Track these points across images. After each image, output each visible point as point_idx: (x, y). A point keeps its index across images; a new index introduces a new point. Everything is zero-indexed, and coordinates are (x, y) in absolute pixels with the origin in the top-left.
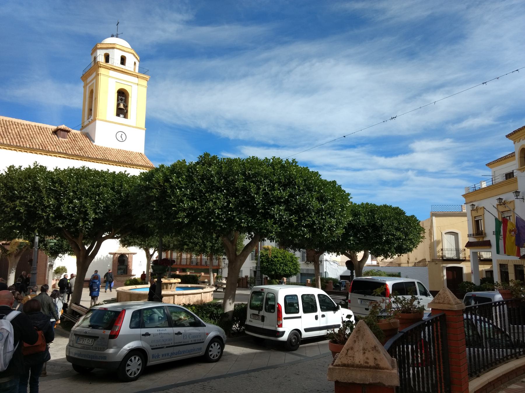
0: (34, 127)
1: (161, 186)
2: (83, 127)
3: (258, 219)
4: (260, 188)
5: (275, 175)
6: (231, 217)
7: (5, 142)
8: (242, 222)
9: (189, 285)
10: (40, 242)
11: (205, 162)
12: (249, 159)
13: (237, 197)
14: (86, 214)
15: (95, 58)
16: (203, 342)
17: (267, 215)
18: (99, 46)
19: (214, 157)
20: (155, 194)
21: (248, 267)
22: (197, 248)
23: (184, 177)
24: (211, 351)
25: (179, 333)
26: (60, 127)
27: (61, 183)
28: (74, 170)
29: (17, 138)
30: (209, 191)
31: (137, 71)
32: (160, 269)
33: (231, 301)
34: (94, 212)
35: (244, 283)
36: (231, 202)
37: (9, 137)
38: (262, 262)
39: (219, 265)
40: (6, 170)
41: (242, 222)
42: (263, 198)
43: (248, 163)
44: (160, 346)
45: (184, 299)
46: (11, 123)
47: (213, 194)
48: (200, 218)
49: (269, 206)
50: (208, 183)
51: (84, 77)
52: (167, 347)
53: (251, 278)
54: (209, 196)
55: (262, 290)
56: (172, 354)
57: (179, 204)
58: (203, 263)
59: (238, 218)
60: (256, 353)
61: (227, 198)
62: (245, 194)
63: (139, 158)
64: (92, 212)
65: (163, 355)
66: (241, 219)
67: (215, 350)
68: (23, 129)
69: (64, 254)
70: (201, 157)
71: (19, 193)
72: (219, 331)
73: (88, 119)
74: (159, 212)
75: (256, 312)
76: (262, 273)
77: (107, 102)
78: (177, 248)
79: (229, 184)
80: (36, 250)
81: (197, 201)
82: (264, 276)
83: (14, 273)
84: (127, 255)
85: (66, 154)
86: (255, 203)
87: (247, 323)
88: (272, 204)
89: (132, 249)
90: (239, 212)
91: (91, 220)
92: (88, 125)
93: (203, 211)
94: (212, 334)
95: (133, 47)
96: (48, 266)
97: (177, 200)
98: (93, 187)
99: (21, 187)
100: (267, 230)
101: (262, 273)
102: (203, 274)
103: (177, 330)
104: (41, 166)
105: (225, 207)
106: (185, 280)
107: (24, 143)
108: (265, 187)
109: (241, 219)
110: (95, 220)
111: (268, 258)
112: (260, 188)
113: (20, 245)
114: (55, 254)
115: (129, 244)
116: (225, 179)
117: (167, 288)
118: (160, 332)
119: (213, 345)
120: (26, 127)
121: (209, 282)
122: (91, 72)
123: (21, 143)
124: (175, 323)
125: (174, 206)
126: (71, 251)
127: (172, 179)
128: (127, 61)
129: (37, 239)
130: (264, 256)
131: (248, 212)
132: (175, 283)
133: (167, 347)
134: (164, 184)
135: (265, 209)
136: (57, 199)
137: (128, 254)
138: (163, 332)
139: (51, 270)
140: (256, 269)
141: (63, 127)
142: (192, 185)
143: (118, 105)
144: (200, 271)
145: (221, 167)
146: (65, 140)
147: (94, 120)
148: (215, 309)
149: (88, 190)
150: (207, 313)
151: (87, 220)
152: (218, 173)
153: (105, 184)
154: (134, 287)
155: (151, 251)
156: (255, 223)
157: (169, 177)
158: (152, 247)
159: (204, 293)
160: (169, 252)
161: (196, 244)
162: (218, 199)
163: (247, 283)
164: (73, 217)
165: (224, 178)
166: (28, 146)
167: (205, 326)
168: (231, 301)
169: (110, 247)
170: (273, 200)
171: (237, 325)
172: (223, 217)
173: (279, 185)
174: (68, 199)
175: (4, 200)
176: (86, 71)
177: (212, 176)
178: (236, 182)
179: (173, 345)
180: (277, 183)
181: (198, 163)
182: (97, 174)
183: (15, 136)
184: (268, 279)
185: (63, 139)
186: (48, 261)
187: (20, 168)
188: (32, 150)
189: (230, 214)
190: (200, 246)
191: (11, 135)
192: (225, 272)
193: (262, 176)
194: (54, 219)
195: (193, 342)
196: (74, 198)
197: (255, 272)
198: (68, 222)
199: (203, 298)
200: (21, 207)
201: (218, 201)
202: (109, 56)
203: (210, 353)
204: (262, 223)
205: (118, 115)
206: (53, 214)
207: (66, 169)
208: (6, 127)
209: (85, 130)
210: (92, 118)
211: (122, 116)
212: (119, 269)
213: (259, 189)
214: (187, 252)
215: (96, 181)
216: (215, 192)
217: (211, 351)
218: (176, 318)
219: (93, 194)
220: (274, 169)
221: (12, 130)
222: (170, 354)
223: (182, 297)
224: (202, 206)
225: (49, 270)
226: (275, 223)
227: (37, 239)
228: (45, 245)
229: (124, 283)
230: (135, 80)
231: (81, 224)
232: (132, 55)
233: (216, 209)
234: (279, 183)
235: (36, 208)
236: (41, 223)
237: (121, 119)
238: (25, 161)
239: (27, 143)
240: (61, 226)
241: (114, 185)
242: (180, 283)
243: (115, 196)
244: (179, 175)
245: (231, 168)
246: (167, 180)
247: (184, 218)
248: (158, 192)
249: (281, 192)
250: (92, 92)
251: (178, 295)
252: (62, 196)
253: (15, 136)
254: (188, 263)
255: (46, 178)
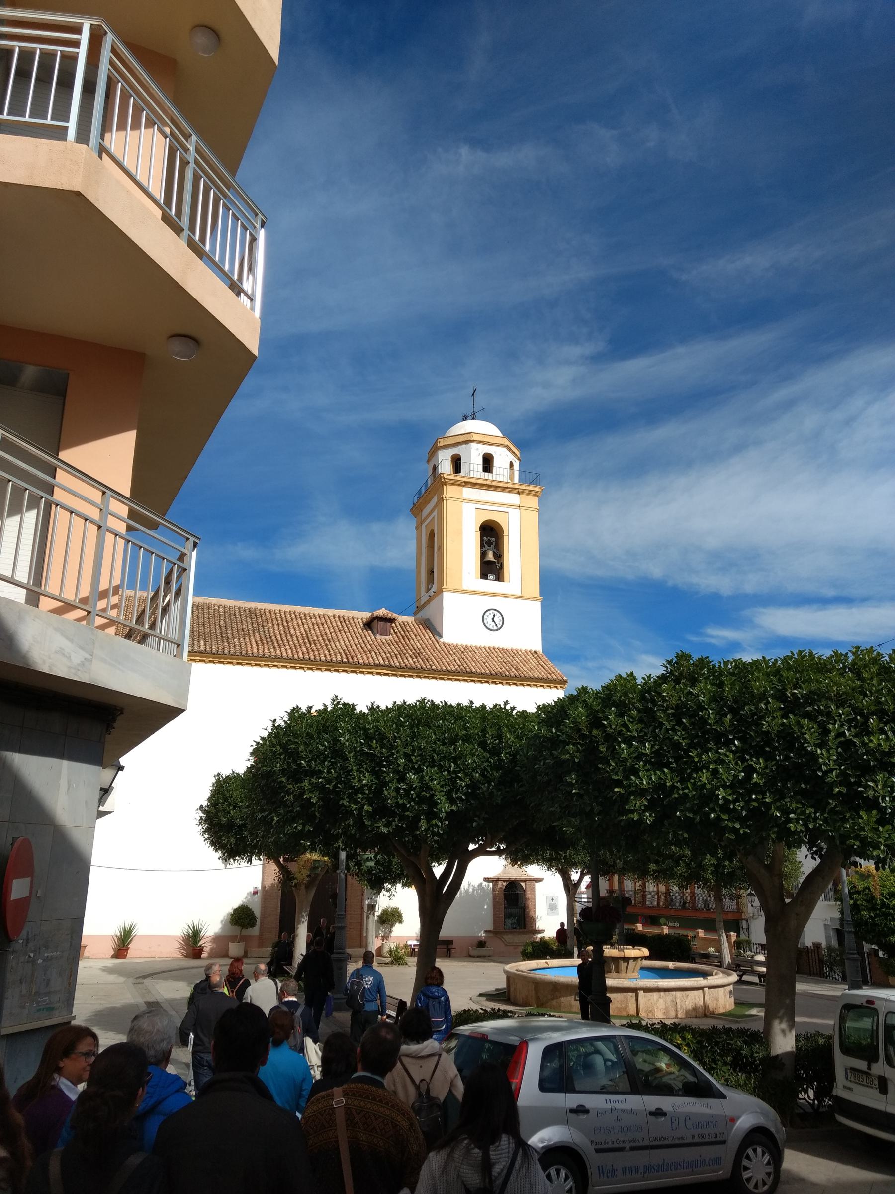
0: (332, 618)
1: (583, 737)
2: (419, 609)
3: (833, 811)
4: (829, 731)
5: (865, 695)
6: (758, 808)
7: (285, 654)
8: (790, 821)
9: (671, 965)
10: (348, 857)
11: (681, 674)
12: (791, 658)
13: (769, 757)
14: (432, 803)
15: (435, 468)
16: (723, 1142)
17: (855, 801)
18: (442, 443)
19: (701, 660)
20: (572, 755)
21: (819, 926)
22: (681, 869)
23: (635, 713)
24: (746, 1168)
25: (659, 1113)
26: (376, 613)
27: (382, 738)
28: (405, 709)
29: (305, 643)
30: (698, 745)
31: (516, 480)
32: (594, 926)
33: (784, 1026)
34: (447, 799)
35: (814, 964)
36: (755, 770)
37: (291, 643)
38: (855, 908)
39: (739, 911)
40: (286, 718)
41: (790, 821)
42: (839, 754)
43: (789, 668)
44: (615, 1145)
45: (661, 1001)
46: (293, 616)
47: (707, 750)
48: (681, 811)
49: (859, 777)
50: (693, 724)
51: (417, 509)
52: (633, 1149)
53: (830, 948)
54: (699, 755)
55: (870, 1002)
56: (648, 1169)
57: (628, 778)
58: (700, 904)
59: (778, 809)
60: (872, 1184)
61: (743, 760)
62: (791, 748)
63: (533, 663)
64: (443, 799)
65: (624, 1171)
66: (786, 812)
67: (757, 1167)
68: (313, 625)
69: (394, 883)
70: (669, 662)
71: (309, 763)
72: (764, 1114)
73: (428, 590)
74: (585, 797)
75: (862, 1065)
76: (860, 938)
77: (463, 550)
78: (634, 870)
79: (746, 725)
80: (342, 876)
81: (671, 769)
82: (867, 947)
83: (306, 924)
84: (523, 884)
85: (389, 667)
86: (821, 769)
87: (839, 1091)
88: (866, 771)
89: (533, 870)
90: (780, 795)
91: (443, 815)
92: (428, 602)
93: (686, 794)
94: (745, 1122)
95: (506, 434)
96: (366, 908)
97: (624, 770)
98: (444, 744)
99: (311, 752)
100: (864, 841)
101: (860, 938)
102: (701, 933)
103: (653, 1102)
104: (345, 704)
105: (742, 783)
106: (662, 949)
107: (316, 653)
108: (842, 726)
109: (786, 812)
110: (450, 815)
111: (873, 898)
112: (829, 731)
113: (315, 866)
114: (377, 885)
115: (525, 860)
116: (734, 711)
117: (618, 971)
118: (613, 1105)
119: (750, 1151)
120: (319, 621)
121: (720, 959)
122: (427, 499)
123: (311, 654)
124: (647, 1080)
125: (618, 783)
126: (407, 876)
127: (607, 719)
128: (497, 463)
129: (343, 855)
130: (858, 892)
131: (803, 793)
132: (635, 959)
133: (633, 1149)
134: (590, 732)
135: (849, 785)
136: (376, 774)
137: (525, 881)
138: (618, 1106)
139: (371, 917)
140: (842, 925)
141: (382, 612)
142: (654, 731)
143: (483, 555)
144: (694, 924)
145: (721, 685)
146: (387, 637)
147: (440, 591)
148: (745, 1042)
149: (434, 751)
150: (725, 1052)
151: (435, 816)
152: (714, 699)
153: (466, 735)
154: (541, 963)
155: (575, 876)
156: (825, 820)
157: (600, 715)
158: (574, 865)
159: (710, 987)
160: (616, 877)
161: (677, 861)
162: (723, 762)
163: (821, 962)
164: (408, 810)
165: (731, 710)
166: (323, 658)
167: (723, 1096)
168: (784, 1026)
169: (485, 869)
170: (868, 761)
171: (811, 1093)
172: (739, 806)
173: (880, 720)
174: (396, 771)
175: (283, 779)
176: (419, 496)
177: (701, 707)
178: (762, 718)
179: (646, 1143)
180: (873, 714)
181: (663, 678)
182: (450, 714)
183: (301, 641)
184: (881, 954)
185: (383, 638)
186: (365, 897)
187: (309, 712)
188: (330, 665)
189: (756, 800)
190: (688, 865)
191: (295, 638)
192: (758, 932)
193: (829, 699)
194: (371, 816)
195: (697, 1140)
196: (407, 769)
197: (840, 933)
198: (399, 821)
199: (708, 1002)
200: (312, 792)
201: (721, 769)
202: (460, 459)
203: (746, 1175)
204: (844, 820)
205: (484, 575)
206: (370, 805)
207: (390, 706)
208: (285, 624)
209: (423, 614)
210: (434, 588)
211: (491, 577)
212: (507, 916)
213: (827, 732)
214: (657, 878)
215: (449, 730)
216: (711, 745)
217: (746, 1168)
218: (647, 1068)
219: (444, 758)
220: (858, 675)
221: (295, 629)
222: (641, 1170)
223: (655, 995)
224: (683, 781)
225: (368, 918)
226: (882, 822)
227: (343, 855)
228: (359, 864)
229: (521, 949)
230: (514, 498)
231: (423, 825)
232: (504, 449)
233: (718, 788)
234: (881, 713)
235: (338, 793)
236: (349, 825)
237: (490, 584)
238: (317, 690)
239: (321, 651)
240: (385, 830)
241: (484, 736)
242: (646, 958)
243: (487, 761)
244: (623, 709)
245: (746, 685)
246: (595, 722)
247: (644, 811)
248: (578, 751)
249: (887, 737)
250: (431, 535)
251: (647, 990)
252: (384, 766)
253: (301, 641)
254: (663, 904)
255: (354, 728)
